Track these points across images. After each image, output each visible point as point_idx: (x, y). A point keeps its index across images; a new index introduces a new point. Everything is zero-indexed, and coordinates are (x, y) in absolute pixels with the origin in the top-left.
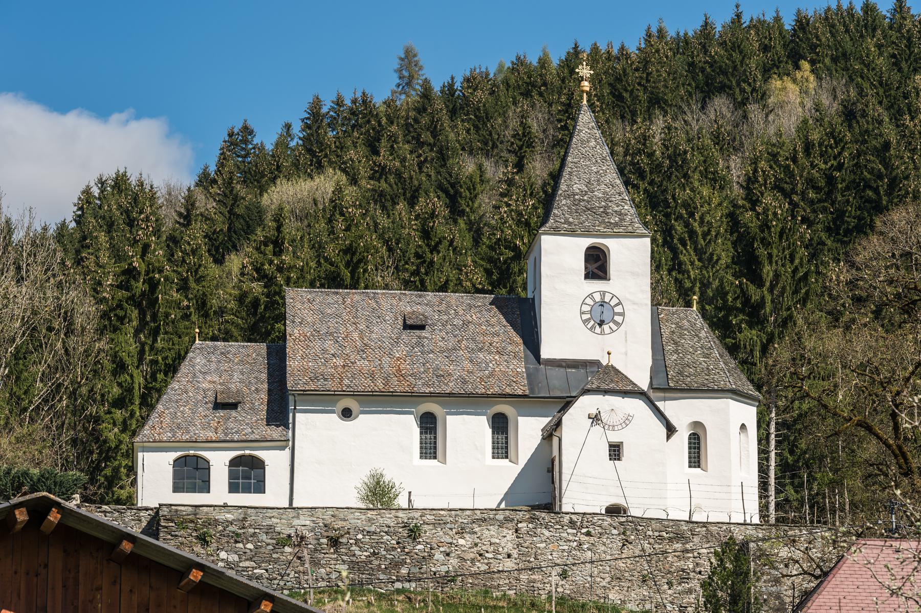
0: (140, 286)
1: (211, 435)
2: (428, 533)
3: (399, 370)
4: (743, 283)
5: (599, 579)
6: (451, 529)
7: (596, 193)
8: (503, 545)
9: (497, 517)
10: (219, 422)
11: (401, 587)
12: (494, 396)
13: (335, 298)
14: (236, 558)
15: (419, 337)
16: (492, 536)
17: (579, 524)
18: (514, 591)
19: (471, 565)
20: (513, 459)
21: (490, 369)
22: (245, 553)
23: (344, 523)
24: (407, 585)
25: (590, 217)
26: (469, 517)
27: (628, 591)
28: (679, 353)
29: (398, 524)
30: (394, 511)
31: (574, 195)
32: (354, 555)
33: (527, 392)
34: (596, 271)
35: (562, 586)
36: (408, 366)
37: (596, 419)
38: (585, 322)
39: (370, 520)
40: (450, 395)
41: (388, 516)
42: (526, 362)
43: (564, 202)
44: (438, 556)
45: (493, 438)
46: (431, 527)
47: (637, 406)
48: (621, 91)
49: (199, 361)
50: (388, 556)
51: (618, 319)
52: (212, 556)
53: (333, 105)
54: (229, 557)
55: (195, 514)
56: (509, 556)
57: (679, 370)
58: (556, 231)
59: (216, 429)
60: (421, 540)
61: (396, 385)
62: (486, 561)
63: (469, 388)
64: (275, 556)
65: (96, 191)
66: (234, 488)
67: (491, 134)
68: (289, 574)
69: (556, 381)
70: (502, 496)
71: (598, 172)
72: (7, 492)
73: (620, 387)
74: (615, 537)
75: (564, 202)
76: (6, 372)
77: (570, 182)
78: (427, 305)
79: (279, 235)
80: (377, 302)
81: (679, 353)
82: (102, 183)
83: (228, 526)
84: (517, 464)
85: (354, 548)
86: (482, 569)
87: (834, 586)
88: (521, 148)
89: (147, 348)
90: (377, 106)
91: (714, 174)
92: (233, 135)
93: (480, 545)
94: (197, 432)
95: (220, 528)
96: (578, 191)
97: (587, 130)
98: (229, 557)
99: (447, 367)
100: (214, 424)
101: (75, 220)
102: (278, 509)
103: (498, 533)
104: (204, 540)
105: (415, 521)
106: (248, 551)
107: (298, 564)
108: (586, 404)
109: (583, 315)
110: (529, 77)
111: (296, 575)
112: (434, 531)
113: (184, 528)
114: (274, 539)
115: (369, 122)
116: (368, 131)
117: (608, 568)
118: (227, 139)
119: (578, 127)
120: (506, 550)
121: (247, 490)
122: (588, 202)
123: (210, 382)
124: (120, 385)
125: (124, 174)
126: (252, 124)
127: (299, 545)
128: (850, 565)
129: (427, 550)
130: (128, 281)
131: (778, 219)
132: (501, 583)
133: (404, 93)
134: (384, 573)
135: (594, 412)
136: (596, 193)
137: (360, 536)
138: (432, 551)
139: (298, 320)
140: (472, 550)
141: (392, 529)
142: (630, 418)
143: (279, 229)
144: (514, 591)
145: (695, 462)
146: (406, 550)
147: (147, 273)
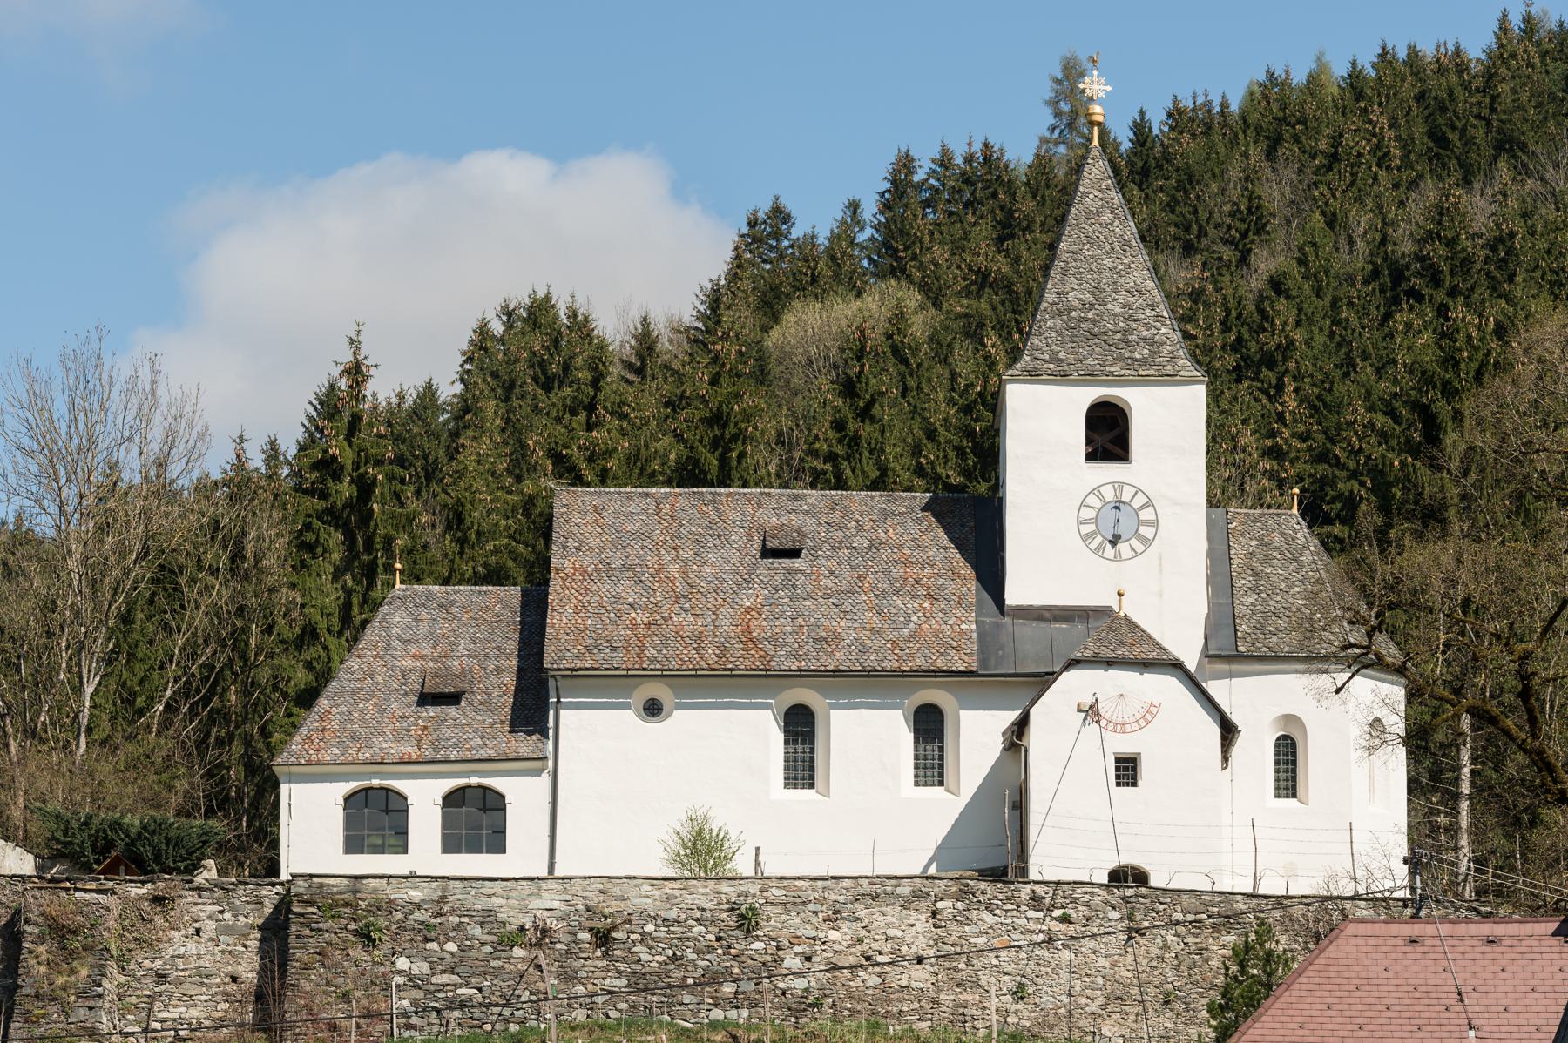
0: (345, 489)
1: (410, 750)
2: (772, 919)
3: (748, 630)
4: (1407, 465)
5: (1083, 1001)
6: (815, 913)
7: (1109, 306)
8: (909, 940)
9: (899, 890)
10: (426, 728)
11: (721, 1017)
12: (915, 673)
13: (643, 503)
14: (426, 968)
15: (789, 571)
16: (889, 925)
17: (1047, 901)
18: (929, 1023)
19: (849, 976)
20: (952, 787)
21: (912, 625)
22: (442, 959)
23: (622, 905)
24: (733, 1014)
25: (1097, 349)
26: (847, 890)
27: (1136, 1021)
28: (1261, 591)
29: (719, 904)
30: (712, 882)
31: (1070, 310)
32: (639, 961)
33: (974, 667)
34: (1110, 446)
35: (1016, 1013)
36: (765, 623)
37: (1091, 712)
38: (1086, 538)
39: (668, 898)
40: (836, 673)
41: (701, 890)
42: (979, 613)
43: (1050, 323)
44: (792, 962)
45: (916, 749)
46: (779, 910)
47: (1166, 687)
48: (1444, 128)
49: (398, 619)
50: (700, 963)
51: (1146, 531)
52: (382, 965)
53: (933, 167)
54: (414, 966)
55: (354, 892)
56: (920, 960)
57: (1258, 621)
58: (1033, 376)
59: (420, 740)
60: (759, 933)
61: (739, 658)
62: (877, 969)
63: (871, 661)
64: (494, 964)
65: (497, 328)
66: (451, 845)
67: (1195, 212)
68: (519, 996)
69: (1029, 644)
70: (932, 853)
71: (1115, 268)
72: (85, 856)
73: (1136, 653)
74: (1113, 923)
75: (1050, 323)
76: (111, 645)
77: (1062, 288)
78: (807, 513)
79: (596, 395)
80: (717, 509)
81: (1261, 591)
82: (509, 314)
83: (412, 912)
84: (957, 794)
85: (638, 948)
86: (870, 983)
87: (1285, 1006)
88: (1244, 235)
89: (355, 600)
90: (1012, 166)
91: (1557, 274)
92: (756, 224)
93: (866, 941)
94: (385, 746)
95: (399, 915)
96: (1077, 303)
97: (1097, 193)
98: (414, 966)
99: (835, 624)
100: (416, 731)
101: (462, 380)
102: (502, 880)
103: (900, 919)
104: (368, 937)
105: (750, 899)
106: (448, 956)
107: (537, 978)
108: (1074, 686)
109: (1081, 527)
110: (1283, 109)
111: (534, 998)
112: (784, 917)
113: (333, 916)
114: (495, 934)
115: (994, 195)
116: (992, 212)
117: (1100, 981)
118: (745, 230)
119: (1081, 189)
120: (914, 949)
121: (474, 847)
122: (1094, 322)
123: (416, 657)
124: (309, 666)
125: (547, 298)
126: (788, 204)
127: (539, 945)
128: (1322, 967)
129: (770, 952)
130: (323, 481)
131: (1473, 347)
132: (905, 1009)
133: (1064, 143)
134: (691, 993)
135: (1088, 700)
136: (1109, 306)
137: (650, 928)
138: (780, 953)
139: (572, 544)
140: (853, 950)
141: (708, 914)
142: (1154, 710)
143: (596, 383)
144: (929, 1023)
145: (1287, 789)
146: (733, 951)
147: (356, 465)
